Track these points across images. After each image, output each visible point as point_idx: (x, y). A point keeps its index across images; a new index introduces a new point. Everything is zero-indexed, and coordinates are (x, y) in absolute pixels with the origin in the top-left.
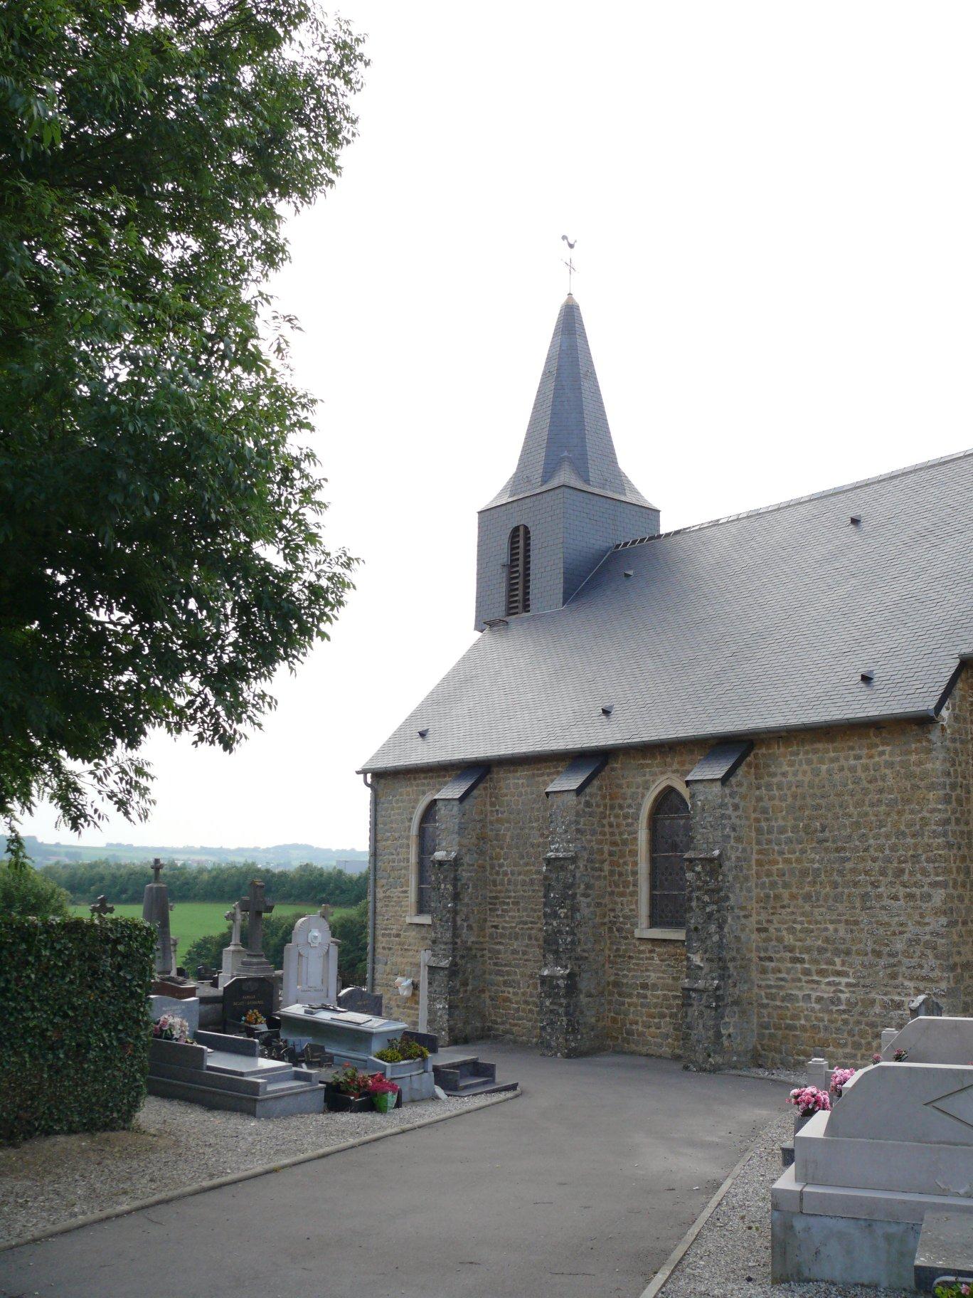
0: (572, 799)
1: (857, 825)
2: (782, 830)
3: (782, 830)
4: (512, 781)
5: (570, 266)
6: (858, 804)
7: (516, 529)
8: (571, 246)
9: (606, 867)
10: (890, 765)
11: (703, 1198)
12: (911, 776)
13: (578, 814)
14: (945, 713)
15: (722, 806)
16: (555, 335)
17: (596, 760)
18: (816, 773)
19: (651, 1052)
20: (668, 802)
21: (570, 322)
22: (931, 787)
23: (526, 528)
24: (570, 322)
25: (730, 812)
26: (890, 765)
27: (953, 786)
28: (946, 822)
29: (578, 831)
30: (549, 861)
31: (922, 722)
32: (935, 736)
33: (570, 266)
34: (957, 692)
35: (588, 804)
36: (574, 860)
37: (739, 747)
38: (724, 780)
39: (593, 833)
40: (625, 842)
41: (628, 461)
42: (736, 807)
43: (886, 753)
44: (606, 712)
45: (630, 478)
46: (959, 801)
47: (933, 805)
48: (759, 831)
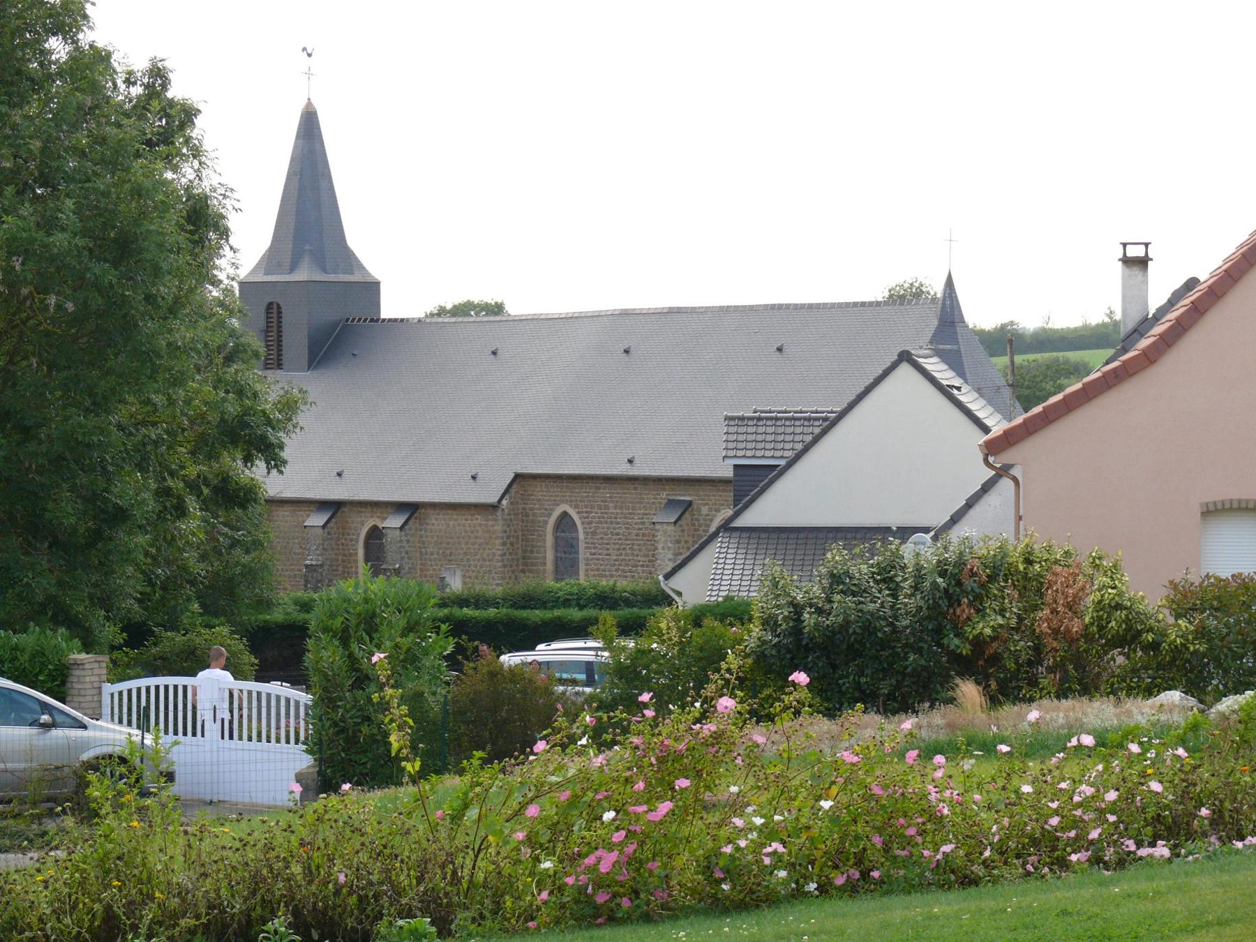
0: (320, 531)
1: (465, 554)
2: (432, 554)
3: (432, 554)
4: (280, 513)
5: (309, 73)
6: (467, 543)
7: (271, 304)
8: (309, 55)
9: (340, 569)
10: (480, 525)
11: (55, 713)
12: (488, 531)
13: (324, 540)
14: (504, 502)
15: (401, 541)
16: (298, 137)
17: (334, 507)
18: (448, 526)
19: (209, 809)
20: (375, 534)
21: (309, 126)
22: (497, 538)
23: (279, 307)
24: (309, 126)
25: (405, 544)
26: (480, 525)
27: (508, 537)
28: (504, 555)
29: (324, 549)
30: (307, 566)
31: (494, 507)
32: (499, 513)
33: (309, 73)
34: (513, 490)
35: (329, 533)
36: (321, 566)
37: (411, 509)
38: (401, 528)
39: (333, 549)
40: (351, 555)
41: (356, 239)
42: (408, 541)
43: (479, 519)
44: (339, 475)
45: (358, 255)
46: (512, 544)
47: (497, 548)
48: (421, 553)
